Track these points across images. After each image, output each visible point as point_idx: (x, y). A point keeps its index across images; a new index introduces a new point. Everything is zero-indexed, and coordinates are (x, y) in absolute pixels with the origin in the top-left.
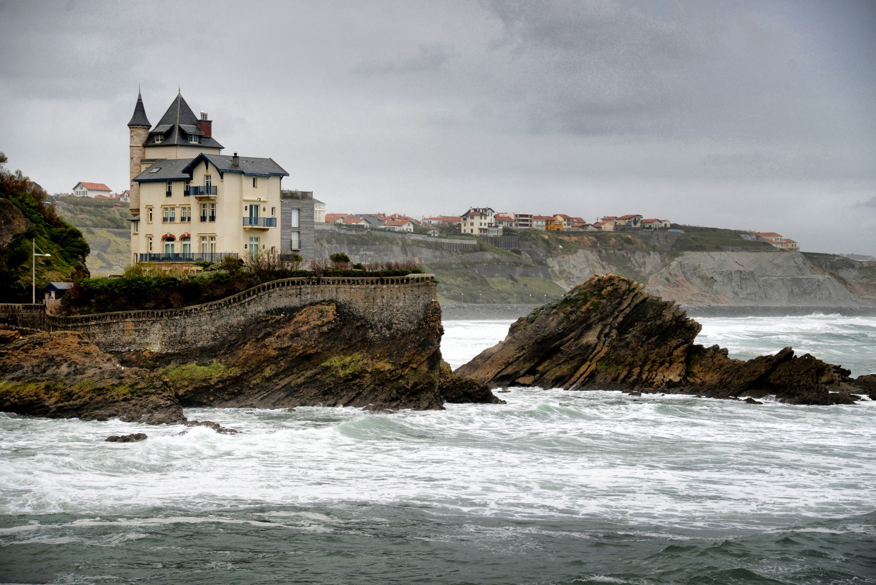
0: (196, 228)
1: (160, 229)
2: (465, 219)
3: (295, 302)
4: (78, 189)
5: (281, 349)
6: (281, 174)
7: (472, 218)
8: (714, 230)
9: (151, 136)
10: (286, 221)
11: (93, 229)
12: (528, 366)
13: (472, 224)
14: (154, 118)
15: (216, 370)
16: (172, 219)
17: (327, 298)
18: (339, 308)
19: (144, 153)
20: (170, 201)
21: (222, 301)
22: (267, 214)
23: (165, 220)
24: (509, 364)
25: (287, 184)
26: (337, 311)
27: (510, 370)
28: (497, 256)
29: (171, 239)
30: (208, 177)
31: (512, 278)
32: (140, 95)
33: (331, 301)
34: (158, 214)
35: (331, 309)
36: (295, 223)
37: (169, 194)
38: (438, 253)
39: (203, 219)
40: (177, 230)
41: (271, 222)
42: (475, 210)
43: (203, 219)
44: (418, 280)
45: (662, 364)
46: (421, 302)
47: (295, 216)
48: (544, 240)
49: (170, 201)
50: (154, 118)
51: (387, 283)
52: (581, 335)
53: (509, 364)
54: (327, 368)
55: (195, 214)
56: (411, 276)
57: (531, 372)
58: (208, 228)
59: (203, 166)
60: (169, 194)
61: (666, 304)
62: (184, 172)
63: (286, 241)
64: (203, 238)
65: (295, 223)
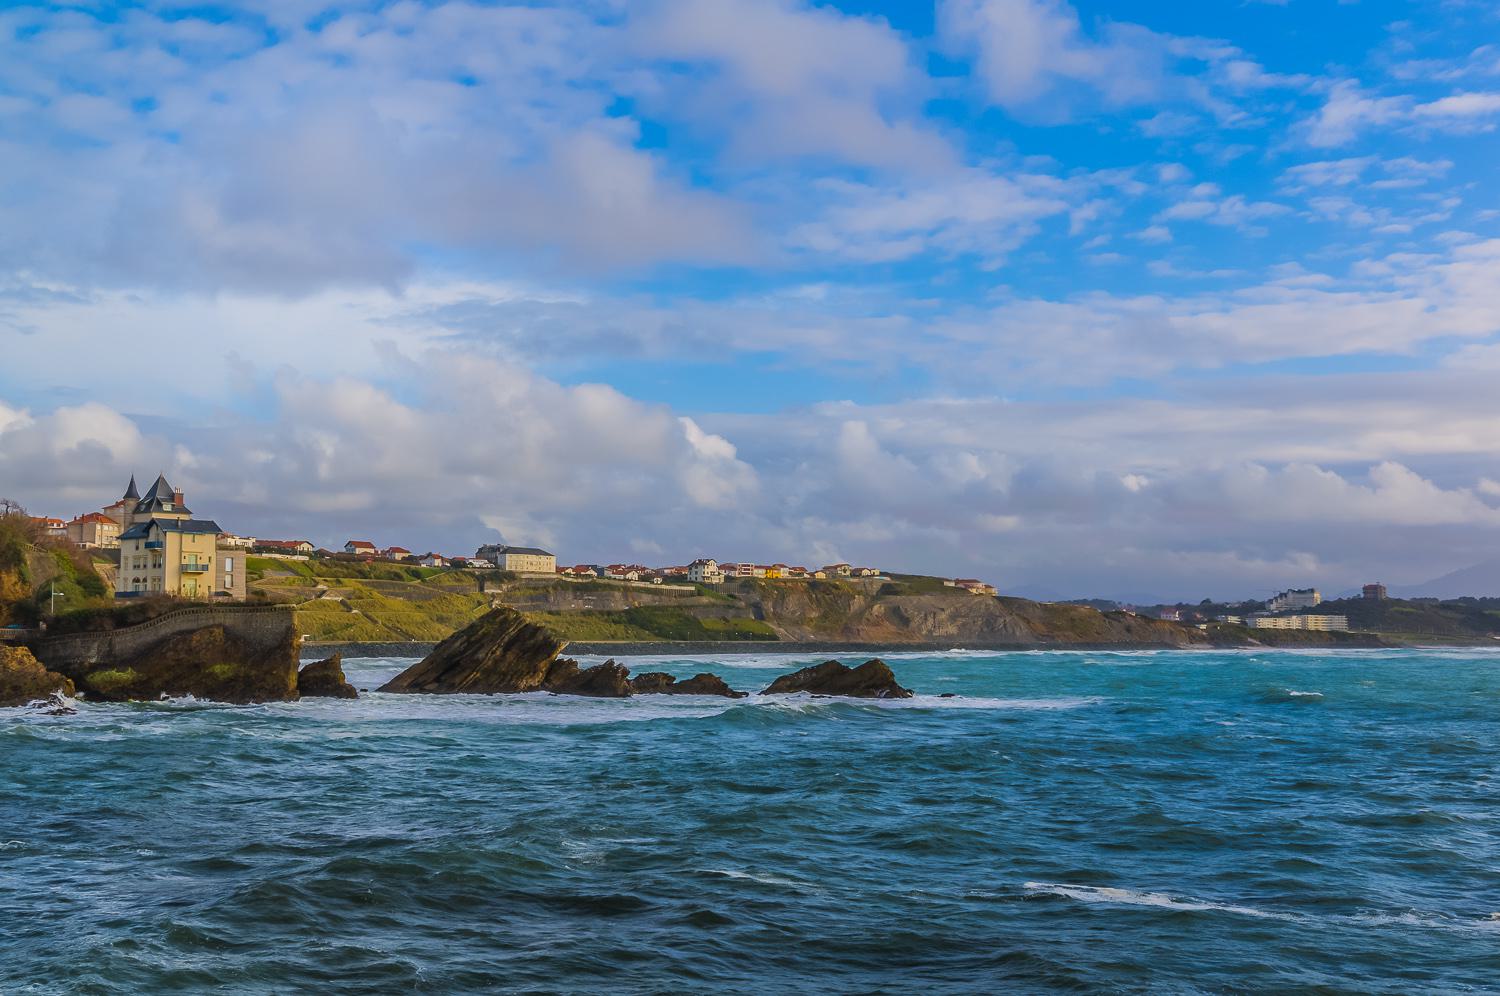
0: (151, 572)
1: (133, 574)
2: (691, 569)
3: (194, 626)
4: (349, 547)
5: (177, 660)
7: (696, 568)
8: (919, 577)
9: (139, 505)
10: (220, 568)
11: (342, 579)
12: (435, 675)
13: (696, 573)
15: (127, 675)
16: (139, 566)
17: (217, 622)
18: (225, 629)
19: (133, 518)
20: (138, 553)
21: (141, 625)
22: (205, 561)
23: (135, 567)
24: (421, 675)
26: (224, 632)
27: (421, 680)
28: (712, 600)
30: (158, 535)
31: (725, 619)
32: (132, 482)
33: (219, 626)
35: (218, 632)
36: (228, 568)
37: (137, 548)
38: (657, 598)
40: (140, 574)
41: (205, 568)
42: (700, 561)
44: (282, 609)
45: (528, 673)
46: (284, 625)
47: (228, 562)
48: (761, 586)
50: (142, 493)
52: (476, 652)
53: (421, 675)
54: (211, 674)
55: (150, 564)
56: (278, 606)
57: (437, 680)
59: (154, 527)
60: (137, 548)
61: (539, 628)
63: (219, 579)
64: (154, 580)
65: (228, 568)
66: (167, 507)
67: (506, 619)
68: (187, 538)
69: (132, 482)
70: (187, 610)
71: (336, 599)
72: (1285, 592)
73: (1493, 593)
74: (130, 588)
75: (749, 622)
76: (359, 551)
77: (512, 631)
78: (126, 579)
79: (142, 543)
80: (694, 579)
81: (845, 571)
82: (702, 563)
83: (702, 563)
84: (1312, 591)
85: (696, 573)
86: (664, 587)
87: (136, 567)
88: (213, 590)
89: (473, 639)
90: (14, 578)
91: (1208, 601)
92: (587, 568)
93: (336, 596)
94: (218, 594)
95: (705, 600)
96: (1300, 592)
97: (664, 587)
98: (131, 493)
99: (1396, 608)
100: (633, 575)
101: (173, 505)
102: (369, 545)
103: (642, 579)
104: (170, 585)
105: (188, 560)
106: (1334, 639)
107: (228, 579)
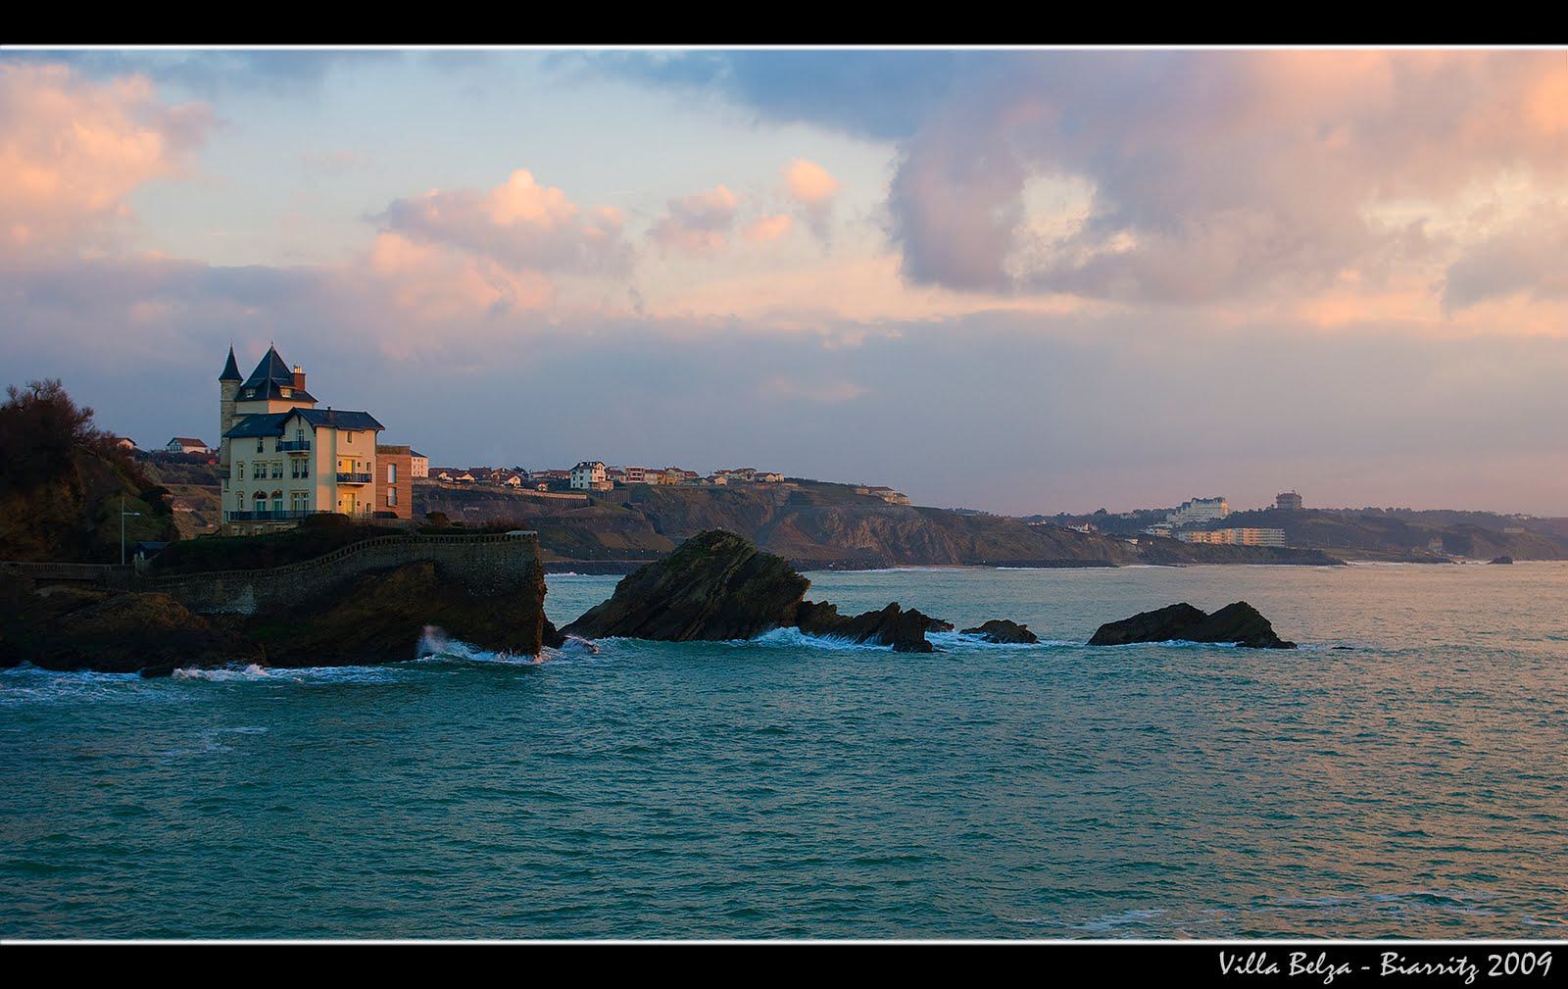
0: (288, 484)
6: (373, 425)
13: (582, 478)
14: (246, 371)
16: (264, 476)
20: (261, 457)
25: (385, 439)
29: (263, 496)
33: (429, 561)
34: (249, 471)
35: (429, 569)
36: (390, 480)
37: (260, 450)
39: (295, 475)
41: (366, 478)
42: (585, 463)
43: (295, 475)
47: (391, 468)
49: (261, 457)
50: (246, 371)
51: (488, 541)
55: (288, 471)
58: (300, 484)
60: (260, 450)
62: (278, 427)
63: (381, 497)
64: (296, 495)
65: (390, 480)
66: (286, 393)
67: (725, 546)
68: (342, 436)
69: (231, 360)
70: (381, 538)
71: (186, 510)
72: (1174, 508)
73: (1559, 512)
74: (249, 506)
75: (1101, 557)
76: (188, 450)
77: (735, 565)
78: (241, 494)
79: (270, 444)
80: (578, 486)
81: (749, 476)
82: (589, 466)
83: (589, 466)
84: (1220, 500)
85: (582, 478)
86: (552, 495)
87: (259, 475)
88: (373, 509)
89: (682, 574)
90: (66, 491)
91: (1103, 511)
92: (442, 471)
93: (185, 507)
94: (378, 515)
95: (598, 511)
96: (1205, 501)
97: (552, 495)
98: (231, 372)
99: (1314, 520)
100: (515, 481)
101: (293, 390)
102: (198, 443)
103: (525, 484)
104: (322, 504)
105: (346, 468)
106: (1275, 556)
107: (390, 493)
